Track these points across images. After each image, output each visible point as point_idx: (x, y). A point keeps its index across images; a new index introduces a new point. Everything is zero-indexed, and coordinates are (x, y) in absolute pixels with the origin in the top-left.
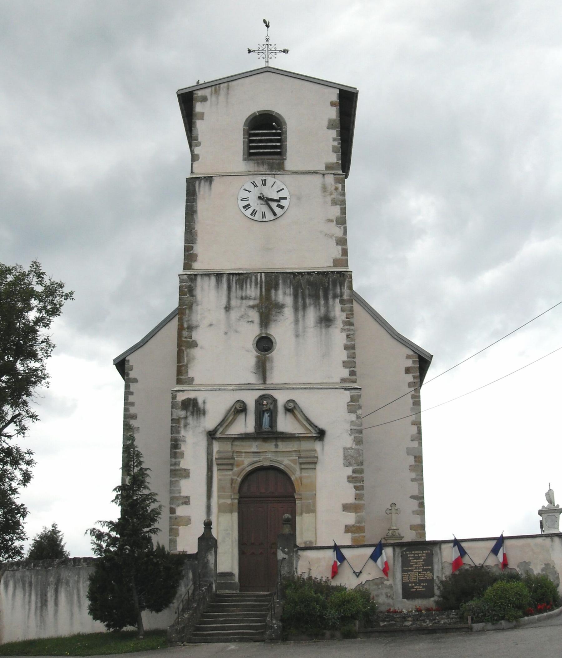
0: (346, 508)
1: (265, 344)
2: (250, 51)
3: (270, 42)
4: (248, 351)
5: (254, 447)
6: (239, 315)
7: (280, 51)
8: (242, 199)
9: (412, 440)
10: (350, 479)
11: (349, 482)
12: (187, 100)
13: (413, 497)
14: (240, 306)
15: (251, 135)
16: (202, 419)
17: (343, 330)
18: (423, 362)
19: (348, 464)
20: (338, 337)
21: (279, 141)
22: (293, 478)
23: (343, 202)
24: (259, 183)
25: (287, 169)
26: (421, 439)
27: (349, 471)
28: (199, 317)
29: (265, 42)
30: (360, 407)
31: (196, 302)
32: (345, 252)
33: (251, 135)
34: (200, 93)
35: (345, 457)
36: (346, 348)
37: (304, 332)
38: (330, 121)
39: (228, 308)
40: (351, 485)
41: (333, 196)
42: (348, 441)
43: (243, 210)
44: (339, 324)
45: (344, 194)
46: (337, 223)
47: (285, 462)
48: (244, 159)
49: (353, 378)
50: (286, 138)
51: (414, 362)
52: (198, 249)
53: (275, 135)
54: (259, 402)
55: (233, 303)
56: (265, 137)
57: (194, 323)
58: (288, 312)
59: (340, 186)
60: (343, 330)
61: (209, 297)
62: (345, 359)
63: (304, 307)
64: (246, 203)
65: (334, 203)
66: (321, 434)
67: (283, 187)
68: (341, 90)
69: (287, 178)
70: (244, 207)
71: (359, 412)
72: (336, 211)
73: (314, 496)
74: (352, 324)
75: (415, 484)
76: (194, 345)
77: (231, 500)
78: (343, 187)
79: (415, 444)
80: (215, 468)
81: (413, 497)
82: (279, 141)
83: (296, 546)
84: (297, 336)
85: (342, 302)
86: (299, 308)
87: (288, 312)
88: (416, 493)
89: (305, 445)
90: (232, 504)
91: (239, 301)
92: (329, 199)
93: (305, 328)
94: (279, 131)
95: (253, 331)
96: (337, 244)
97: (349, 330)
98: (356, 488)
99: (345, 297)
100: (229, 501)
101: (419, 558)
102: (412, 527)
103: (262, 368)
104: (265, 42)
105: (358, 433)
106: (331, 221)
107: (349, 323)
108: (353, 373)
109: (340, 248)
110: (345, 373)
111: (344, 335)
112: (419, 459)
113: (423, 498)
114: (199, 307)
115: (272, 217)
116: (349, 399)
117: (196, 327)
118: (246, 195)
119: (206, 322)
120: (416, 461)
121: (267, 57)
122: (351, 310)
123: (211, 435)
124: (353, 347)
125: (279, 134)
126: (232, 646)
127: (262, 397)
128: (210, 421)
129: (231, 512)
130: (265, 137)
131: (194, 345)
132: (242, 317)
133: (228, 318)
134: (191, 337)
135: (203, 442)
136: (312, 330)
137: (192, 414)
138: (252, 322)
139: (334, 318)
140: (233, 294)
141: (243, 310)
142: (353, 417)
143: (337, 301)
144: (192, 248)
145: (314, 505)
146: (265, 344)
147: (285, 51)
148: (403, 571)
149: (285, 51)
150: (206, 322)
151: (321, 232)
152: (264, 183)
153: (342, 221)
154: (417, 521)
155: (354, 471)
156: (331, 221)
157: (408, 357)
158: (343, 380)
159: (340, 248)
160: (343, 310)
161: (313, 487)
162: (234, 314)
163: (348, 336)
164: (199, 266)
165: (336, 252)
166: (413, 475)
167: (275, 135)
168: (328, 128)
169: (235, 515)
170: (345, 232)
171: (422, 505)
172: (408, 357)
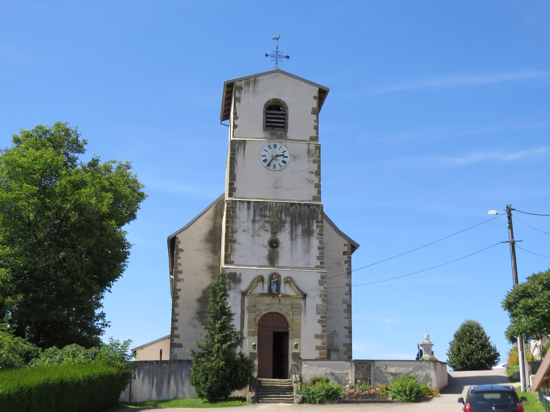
0: (317, 336)
1: (274, 244)
2: (266, 55)
3: (279, 50)
4: (265, 247)
5: (268, 300)
6: (260, 226)
7: (285, 57)
8: (263, 156)
9: (346, 295)
10: (319, 322)
11: (319, 322)
12: (230, 88)
13: (345, 328)
14: (261, 221)
15: (267, 114)
16: (239, 285)
17: (317, 238)
18: (353, 247)
19: (318, 313)
20: (315, 242)
21: (283, 119)
22: (288, 319)
23: (319, 162)
24: (272, 147)
25: (289, 138)
26: (351, 294)
27: (319, 317)
28: (237, 226)
29: (275, 50)
30: (326, 282)
31: (236, 216)
32: (319, 192)
33: (267, 114)
34: (238, 84)
35: (317, 309)
36: (319, 248)
37: (296, 238)
38: (313, 109)
39: (254, 221)
40: (320, 325)
41: (314, 158)
42: (319, 301)
43: (263, 163)
44: (316, 235)
45: (319, 157)
46: (316, 174)
47: (284, 310)
48: (263, 130)
49: (322, 265)
50: (288, 118)
51: (348, 248)
52: (237, 185)
53: (280, 114)
54: (271, 278)
55: (257, 218)
56: (275, 116)
57: (235, 229)
58: (287, 226)
59: (318, 151)
60: (317, 238)
61: (244, 216)
62: (318, 255)
63: (296, 225)
64: (264, 158)
65: (314, 162)
66: (305, 296)
67: (285, 149)
68: (319, 89)
69: (289, 144)
70: (264, 161)
71: (325, 285)
72: (314, 167)
73: (299, 330)
74: (322, 235)
75: (347, 320)
76: (234, 242)
77: (255, 329)
78: (320, 152)
79: (348, 297)
80: (246, 312)
81: (345, 328)
82: (283, 119)
83: (301, 359)
84: (292, 240)
85: (317, 222)
86: (293, 225)
87: (287, 226)
88: (347, 325)
89: (296, 301)
90: (255, 331)
91: (260, 218)
92: (312, 159)
93: (296, 235)
94: (283, 113)
95: (267, 237)
96: (315, 187)
97: (321, 238)
98: (322, 326)
99: (319, 219)
100: (253, 330)
101: (364, 367)
102: (344, 345)
103: (272, 259)
104: (275, 50)
105: (325, 297)
106: (312, 173)
107: (321, 234)
108: (322, 263)
109: (317, 189)
110: (318, 263)
111: (318, 241)
112: (349, 306)
113: (351, 328)
114: (238, 220)
115: (280, 168)
116: (320, 278)
117: (236, 231)
118: (264, 153)
119: (241, 229)
120: (347, 307)
121: (277, 59)
122: (322, 227)
123: (244, 294)
124: (322, 248)
125: (284, 115)
126: (281, 404)
127: (273, 274)
128: (244, 286)
129: (254, 336)
130: (275, 116)
131: (234, 242)
132: (261, 227)
133: (254, 227)
134: (233, 237)
135: (239, 297)
136: (300, 237)
137: (233, 282)
138: (267, 230)
139: (313, 230)
140: (257, 214)
141: (262, 223)
142: (322, 288)
143: (315, 221)
144: (233, 184)
145: (300, 334)
146: (274, 244)
147: (288, 57)
148: (355, 373)
149: (288, 57)
150: (241, 229)
151: (306, 179)
152: (275, 146)
153: (318, 173)
154: (347, 341)
155: (322, 317)
156: (312, 173)
157: (345, 245)
158: (317, 267)
159: (317, 189)
160: (317, 227)
161: (299, 324)
162: (257, 225)
163: (320, 242)
164: (238, 196)
165: (314, 192)
166: (346, 315)
167: (280, 114)
168: (312, 113)
169: (256, 337)
170: (320, 181)
171: (350, 332)
172: (345, 245)
